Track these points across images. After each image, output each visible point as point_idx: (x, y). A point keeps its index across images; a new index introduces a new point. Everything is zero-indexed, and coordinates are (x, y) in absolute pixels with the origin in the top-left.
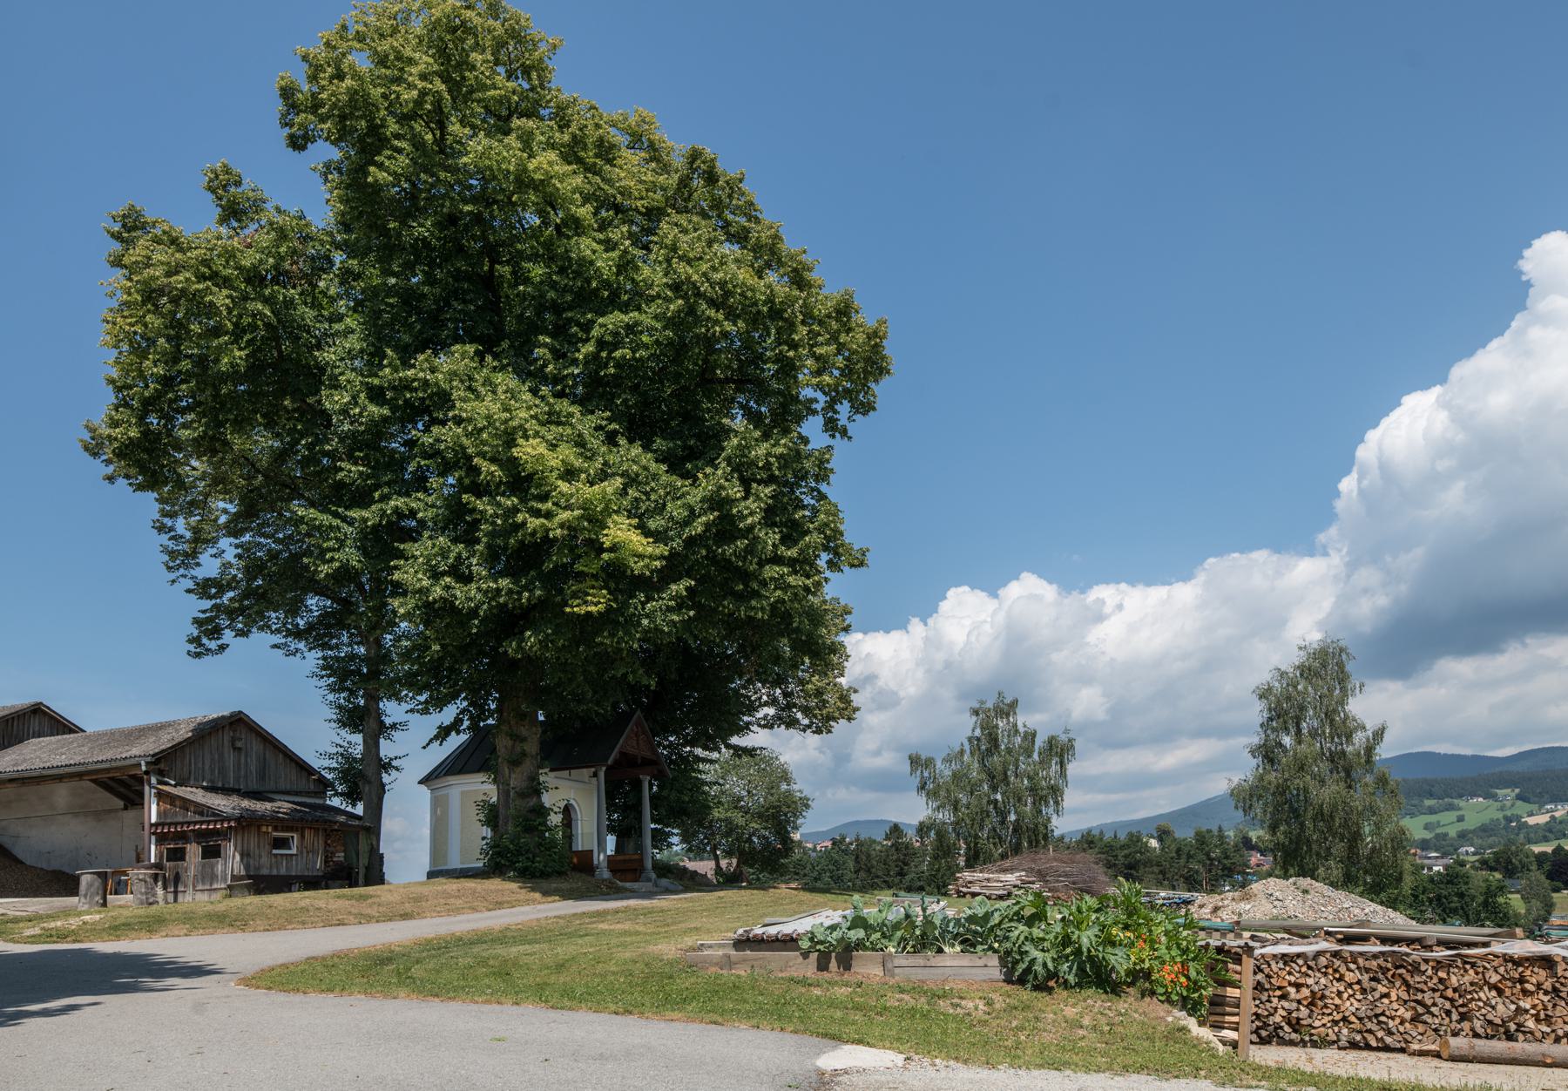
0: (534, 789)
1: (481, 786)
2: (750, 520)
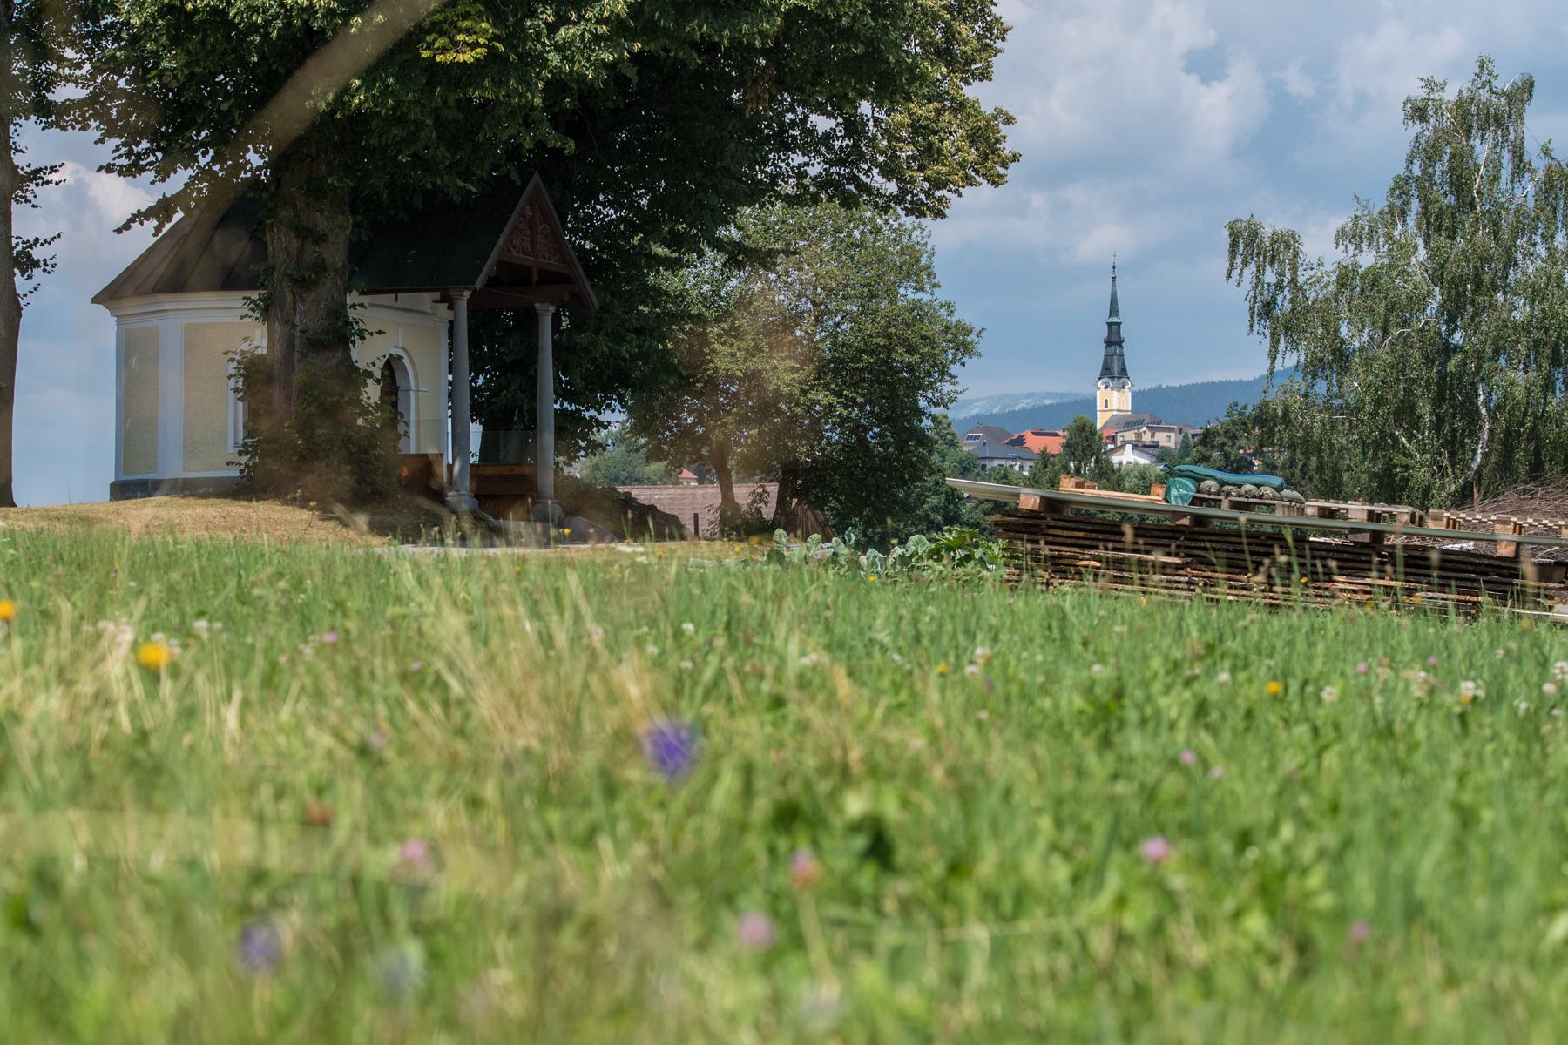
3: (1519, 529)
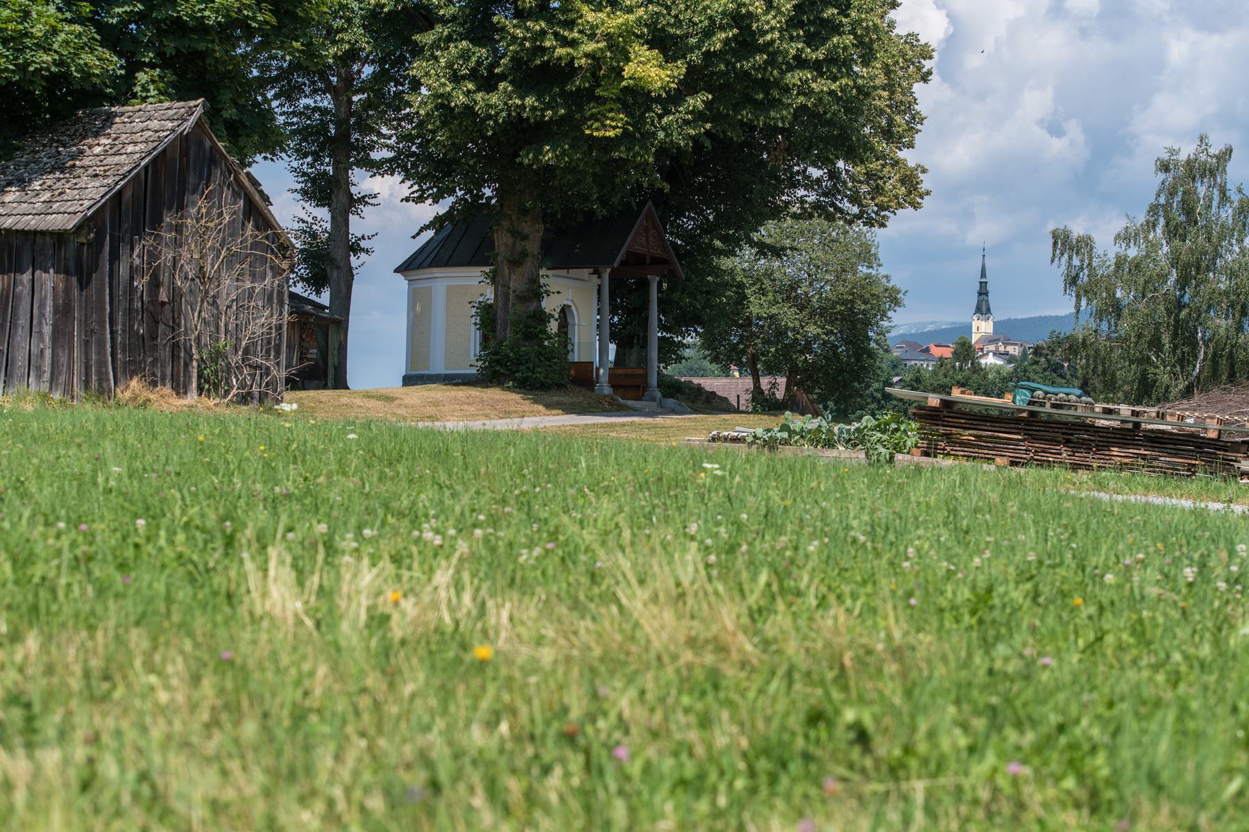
0: (535, 292)
1: (471, 285)
2: (768, 37)
3: (1220, 421)
